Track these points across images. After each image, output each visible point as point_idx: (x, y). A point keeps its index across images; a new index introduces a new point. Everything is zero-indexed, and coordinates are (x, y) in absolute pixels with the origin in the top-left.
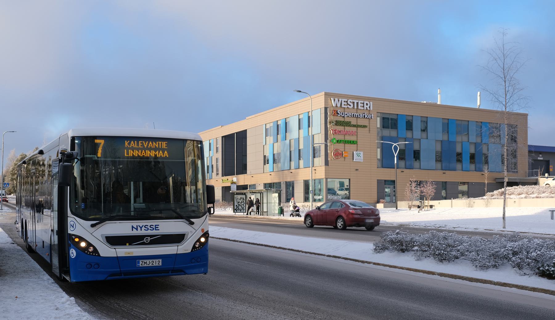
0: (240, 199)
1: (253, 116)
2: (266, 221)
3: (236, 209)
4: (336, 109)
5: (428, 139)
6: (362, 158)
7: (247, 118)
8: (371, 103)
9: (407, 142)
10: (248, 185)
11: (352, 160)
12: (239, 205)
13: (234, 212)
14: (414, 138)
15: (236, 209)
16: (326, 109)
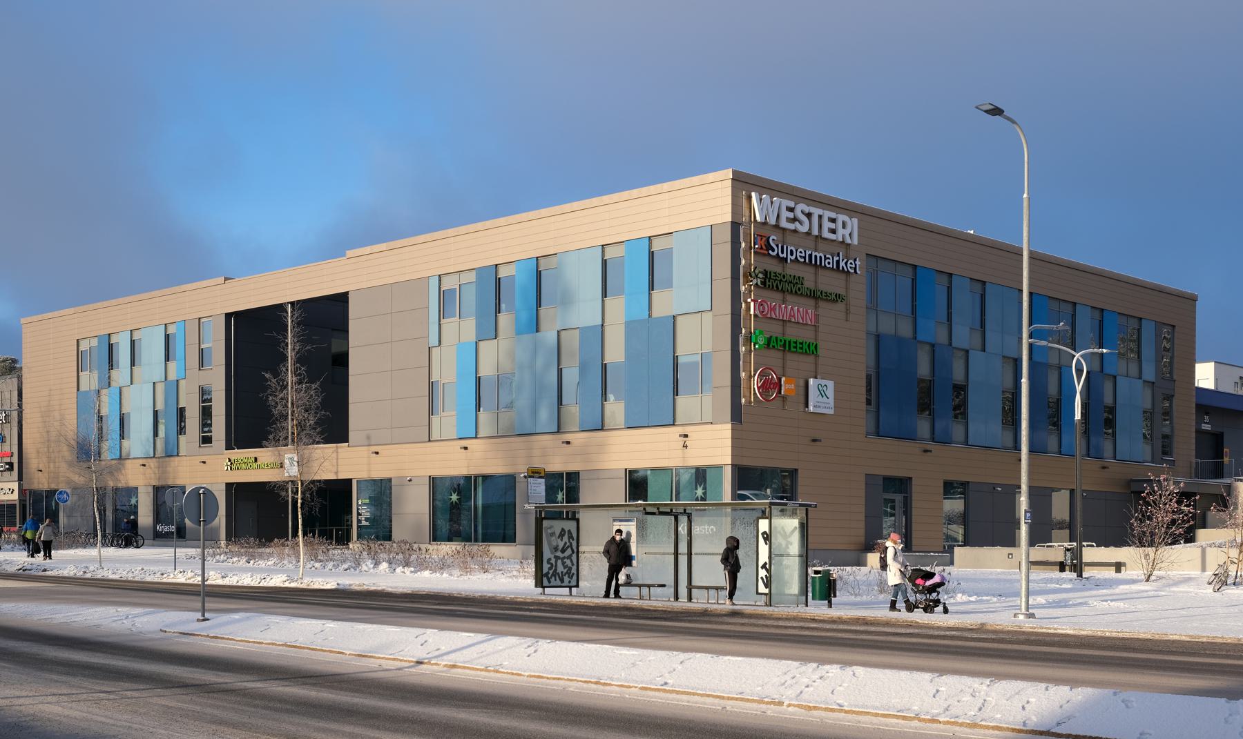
0: (561, 535)
1: (383, 246)
2: (993, 641)
3: (548, 573)
4: (764, 232)
5: (986, 350)
6: (831, 401)
7: (347, 252)
8: (855, 221)
9: (1105, 351)
10: (351, 480)
11: (802, 406)
12: (557, 558)
13: (539, 583)
14: (954, 345)
15: (548, 573)
16: (735, 226)
